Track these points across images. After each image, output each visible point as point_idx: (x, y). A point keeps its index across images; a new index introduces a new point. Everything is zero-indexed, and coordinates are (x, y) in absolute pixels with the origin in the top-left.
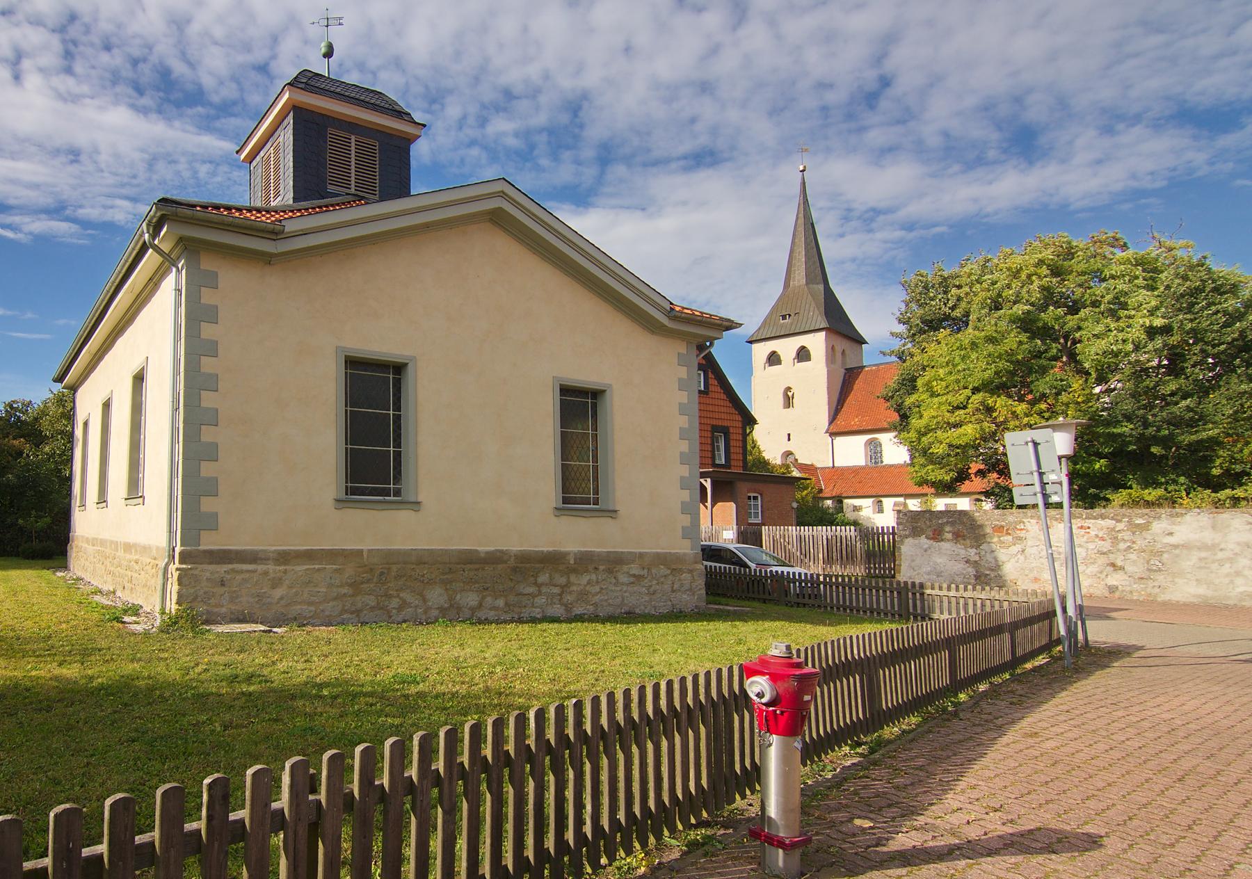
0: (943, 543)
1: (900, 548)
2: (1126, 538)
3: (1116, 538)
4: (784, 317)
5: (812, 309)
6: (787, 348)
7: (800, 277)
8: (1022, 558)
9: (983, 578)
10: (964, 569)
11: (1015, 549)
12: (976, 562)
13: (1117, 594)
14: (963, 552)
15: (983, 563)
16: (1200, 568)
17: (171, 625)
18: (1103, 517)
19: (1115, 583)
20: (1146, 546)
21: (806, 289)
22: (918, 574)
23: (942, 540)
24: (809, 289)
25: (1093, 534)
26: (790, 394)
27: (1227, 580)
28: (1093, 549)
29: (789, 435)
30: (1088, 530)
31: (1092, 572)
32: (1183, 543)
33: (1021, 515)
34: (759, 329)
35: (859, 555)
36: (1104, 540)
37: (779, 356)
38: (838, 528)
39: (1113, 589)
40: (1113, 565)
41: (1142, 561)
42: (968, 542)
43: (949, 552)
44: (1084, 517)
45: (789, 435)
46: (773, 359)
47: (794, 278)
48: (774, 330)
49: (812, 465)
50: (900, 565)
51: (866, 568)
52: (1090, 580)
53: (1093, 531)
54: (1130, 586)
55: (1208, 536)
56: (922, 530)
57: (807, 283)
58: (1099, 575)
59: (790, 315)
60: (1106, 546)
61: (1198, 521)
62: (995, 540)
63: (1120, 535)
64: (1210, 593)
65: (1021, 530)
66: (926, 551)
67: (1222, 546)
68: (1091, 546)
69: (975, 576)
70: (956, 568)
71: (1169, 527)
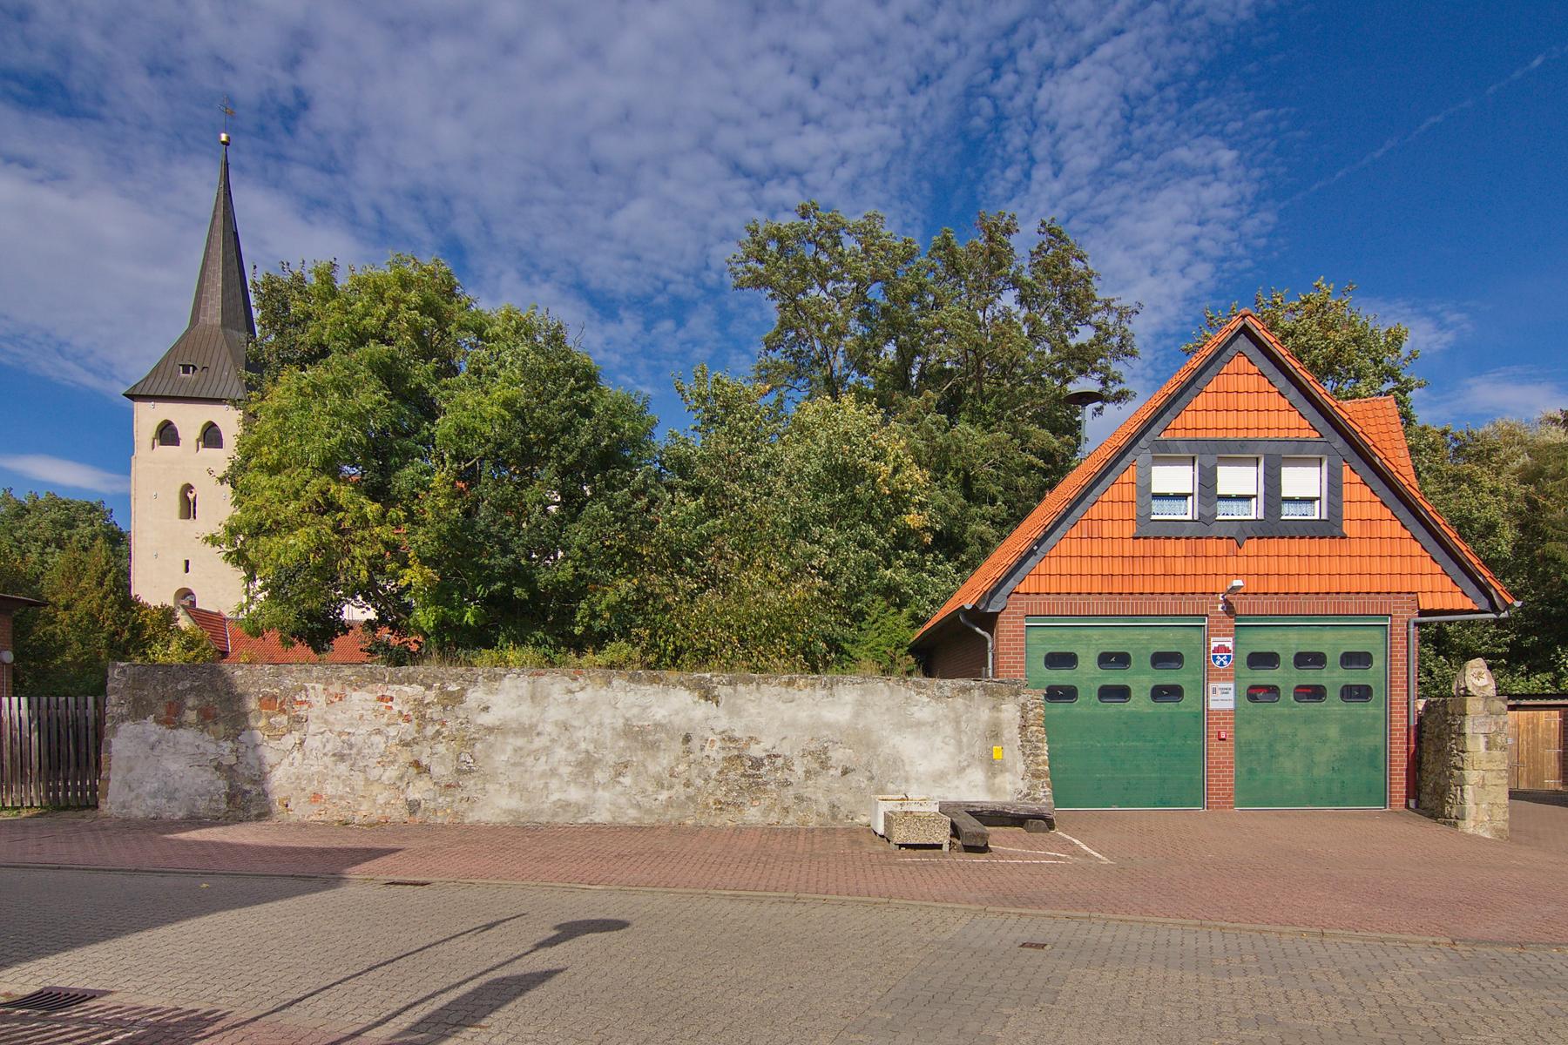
0: (181, 731)
1: (109, 744)
2: (435, 716)
3: (423, 716)
4: (186, 369)
5: (227, 367)
6: (190, 419)
7: (213, 314)
8: (297, 755)
9: (238, 800)
10: (212, 782)
11: (291, 740)
12: (231, 767)
13: (419, 817)
14: (211, 748)
15: (240, 769)
16: (514, 765)
17: (1475, 655)
18: (410, 680)
19: (417, 796)
20: (457, 730)
21: (221, 333)
22: (137, 797)
23: (181, 725)
24: (225, 334)
25: (396, 708)
26: (191, 496)
27: (540, 784)
28: (394, 737)
29: (187, 562)
30: (390, 704)
31: (390, 779)
32: (498, 723)
33: (304, 675)
34: (147, 378)
35: (35, 761)
36: (408, 721)
37: (175, 430)
38: (71, 700)
39: (413, 806)
40: (417, 764)
41: (451, 755)
42: (221, 727)
43: (190, 750)
44: (387, 679)
45: (187, 562)
46: (167, 435)
47: (205, 309)
48: (170, 386)
49: (219, 614)
50: (108, 780)
51: (48, 790)
52: (386, 794)
53: (397, 704)
54: (435, 800)
55: (525, 712)
56: (149, 703)
57: (224, 325)
58: (399, 784)
59: (195, 368)
60: (409, 729)
61: (517, 687)
62: (262, 723)
63: (429, 711)
64: (522, 806)
65: (302, 703)
66: (153, 748)
67: (540, 728)
68: (392, 731)
69: (228, 795)
70: (199, 781)
71: (485, 698)
